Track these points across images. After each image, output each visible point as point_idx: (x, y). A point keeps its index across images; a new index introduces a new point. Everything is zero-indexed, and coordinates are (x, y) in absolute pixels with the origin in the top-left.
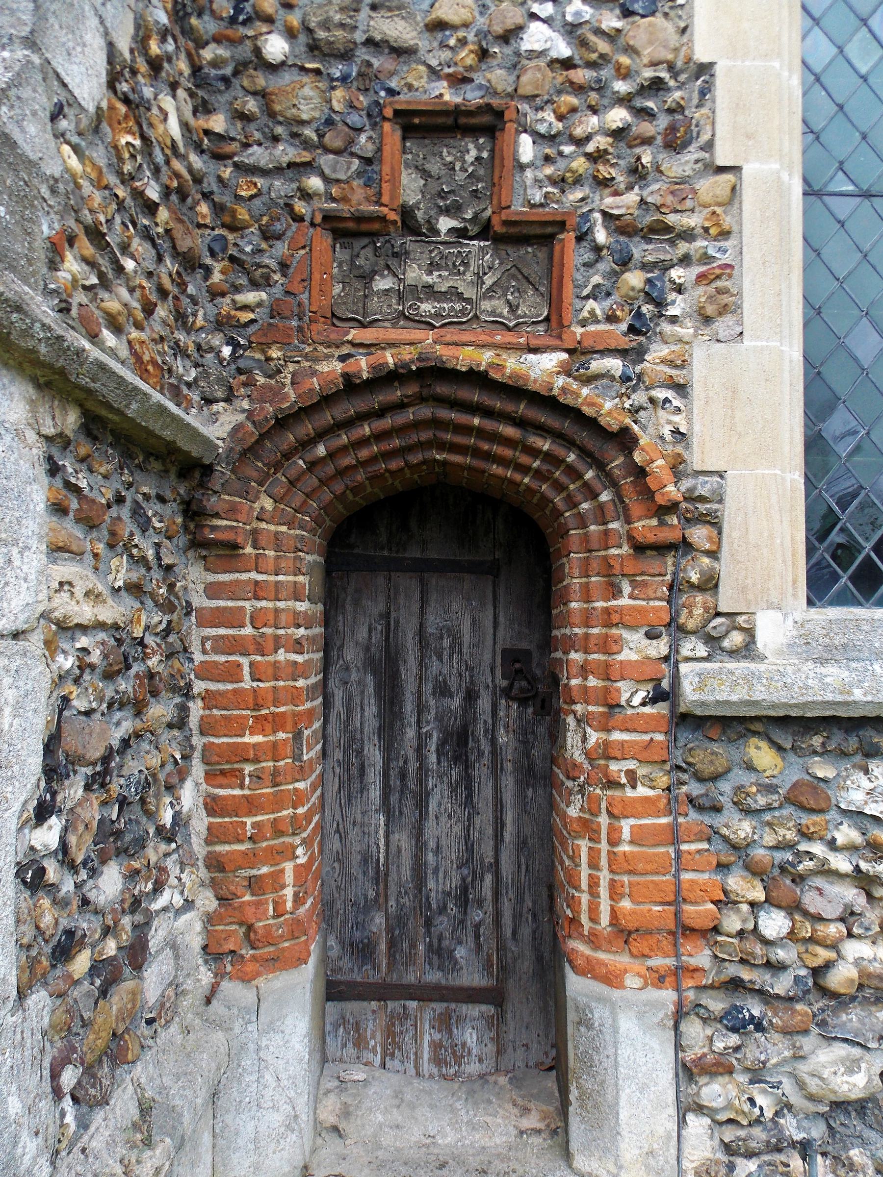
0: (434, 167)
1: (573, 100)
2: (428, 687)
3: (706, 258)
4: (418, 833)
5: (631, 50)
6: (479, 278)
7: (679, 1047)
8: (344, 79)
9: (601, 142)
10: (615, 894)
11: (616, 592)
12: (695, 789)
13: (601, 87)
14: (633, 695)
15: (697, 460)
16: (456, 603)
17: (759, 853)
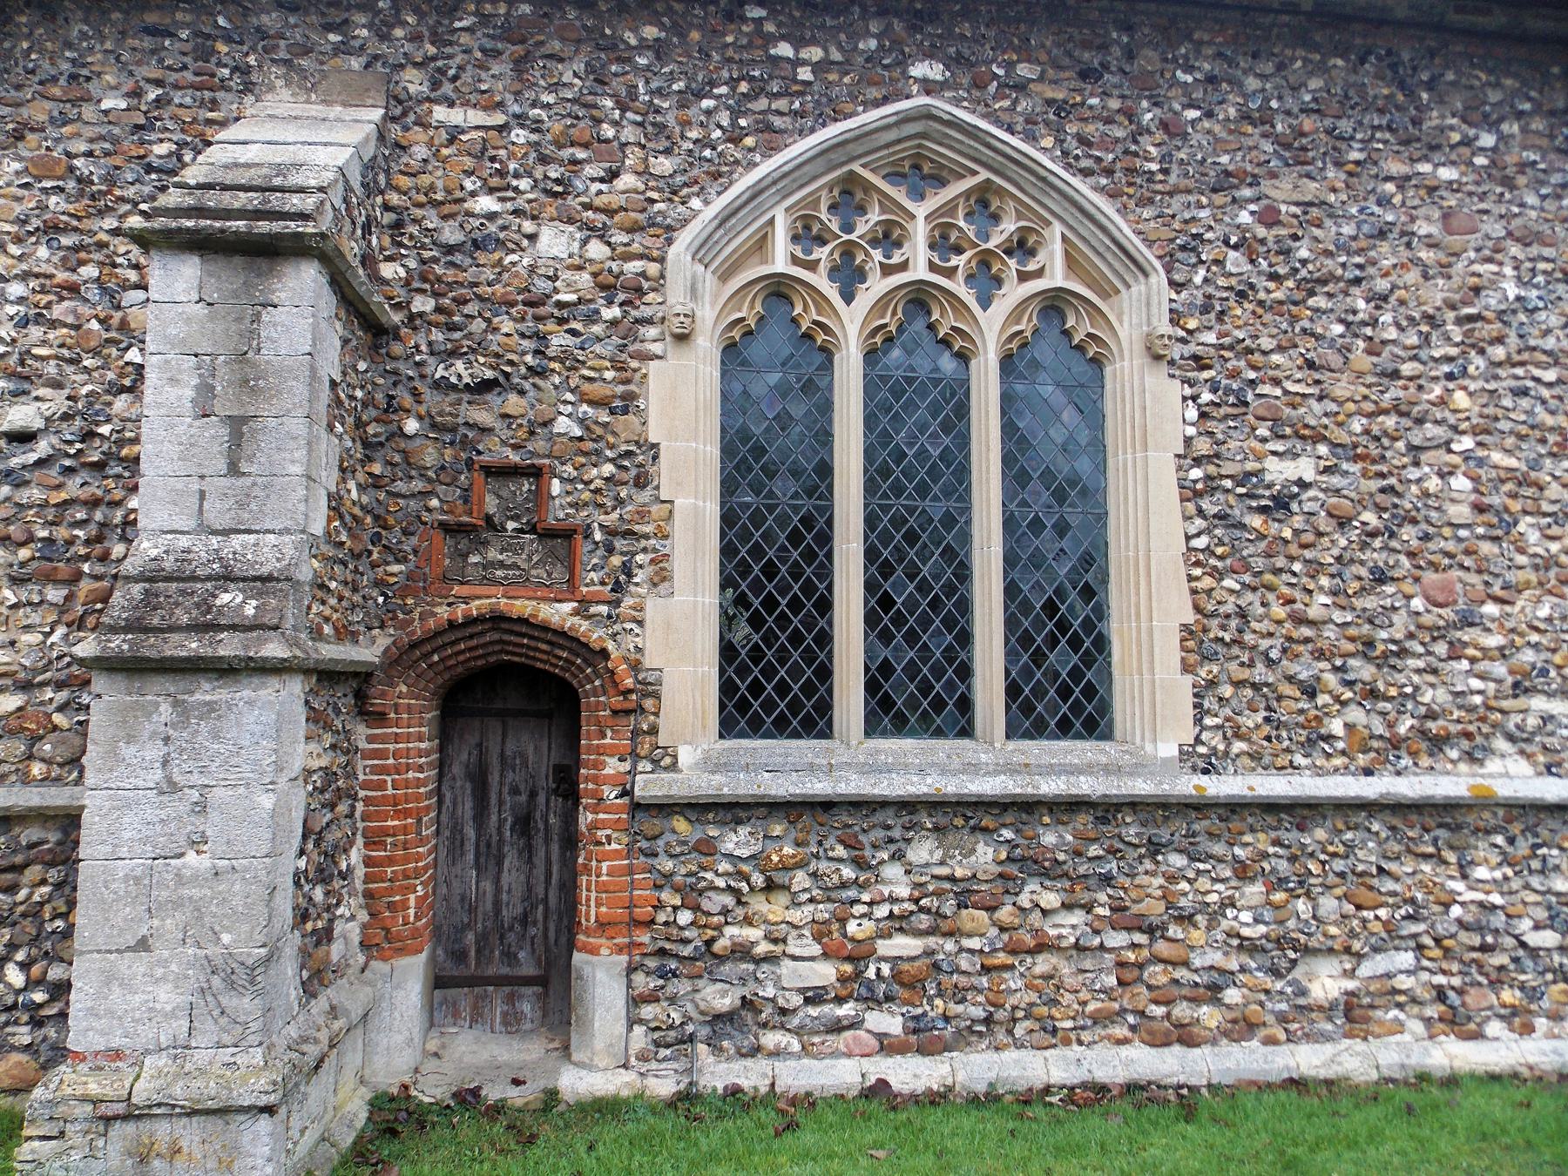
0: (505, 493)
1: (583, 460)
2: (506, 790)
3: (655, 550)
4: (497, 881)
5: (614, 434)
6: (530, 558)
7: (629, 986)
8: (452, 443)
9: (598, 483)
10: (598, 905)
11: (604, 736)
12: (644, 844)
13: (598, 453)
14: (610, 793)
15: (648, 662)
16: (525, 737)
17: (678, 879)
